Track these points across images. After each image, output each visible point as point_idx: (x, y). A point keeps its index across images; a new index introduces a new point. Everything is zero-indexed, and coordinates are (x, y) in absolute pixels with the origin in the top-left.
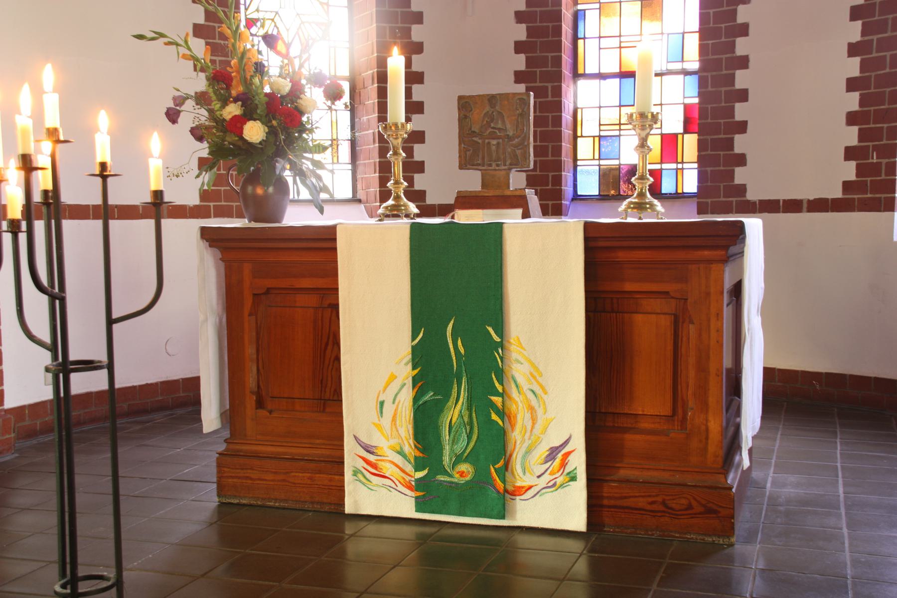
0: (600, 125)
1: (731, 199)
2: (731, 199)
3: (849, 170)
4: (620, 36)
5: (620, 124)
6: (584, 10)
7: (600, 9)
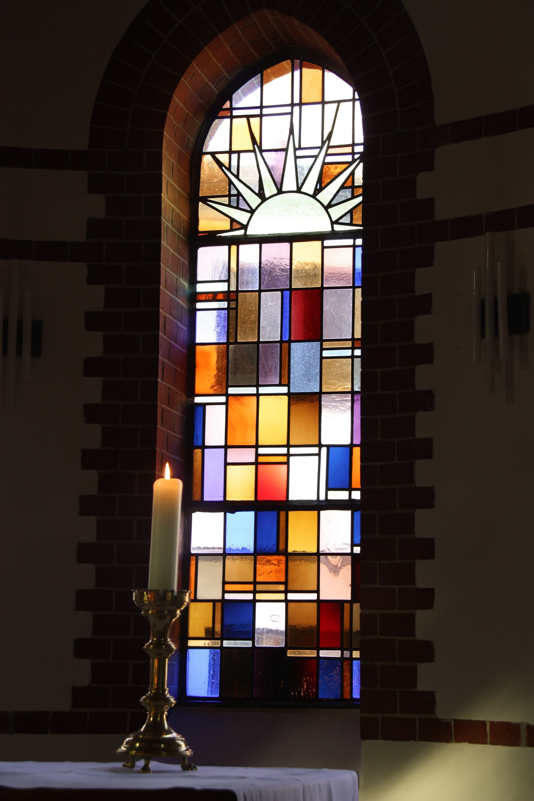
0: (224, 583)
1: (412, 716)
2: (412, 716)
3: (82, 673)
4: (257, 446)
5: (255, 583)
6: (204, 405)
7: (226, 404)
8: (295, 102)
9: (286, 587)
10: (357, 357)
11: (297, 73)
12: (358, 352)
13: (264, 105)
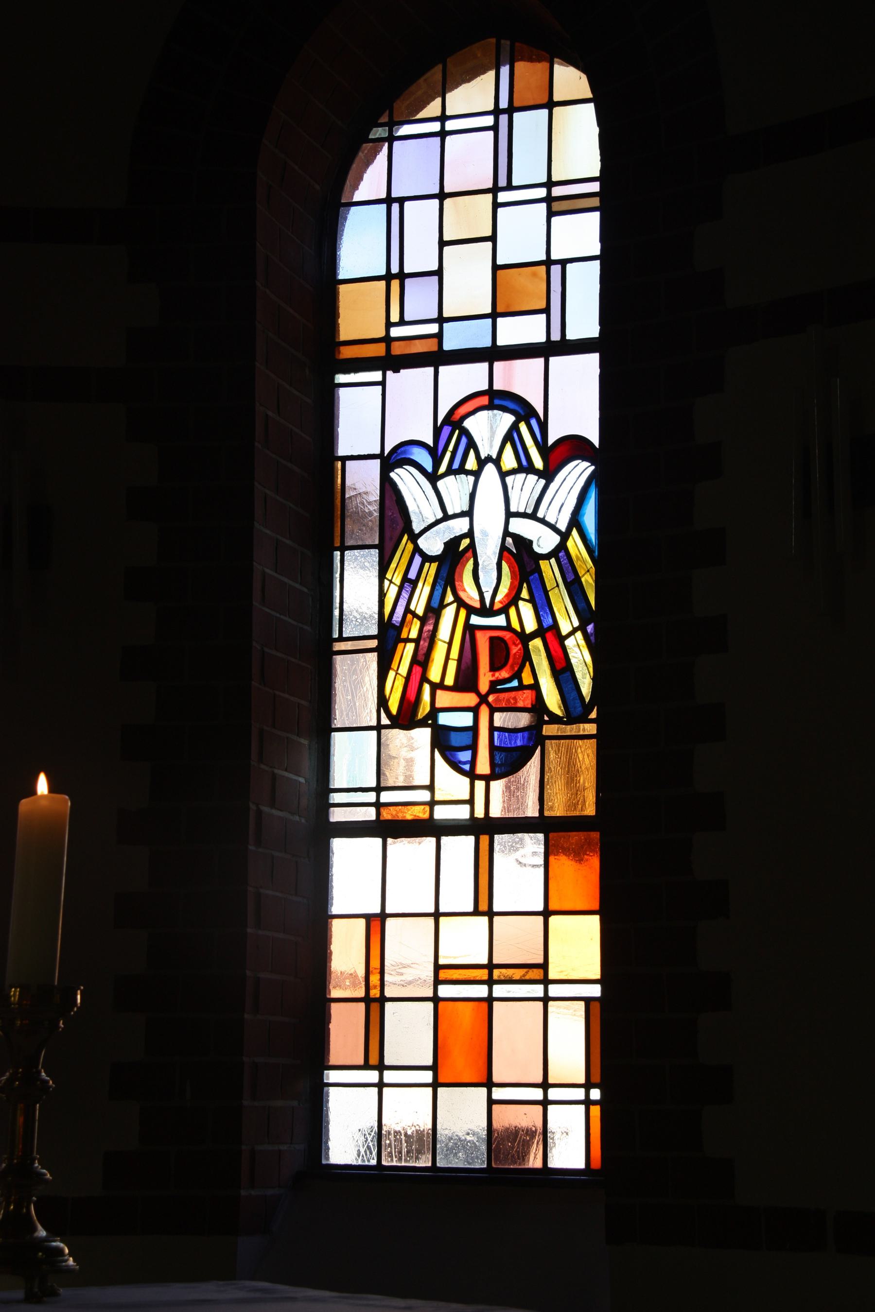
8: (486, 977)
9: (435, 1077)
10: (595, 1103)
11: (505, 71)
12: (595, 1094)
13: (448, 113)
